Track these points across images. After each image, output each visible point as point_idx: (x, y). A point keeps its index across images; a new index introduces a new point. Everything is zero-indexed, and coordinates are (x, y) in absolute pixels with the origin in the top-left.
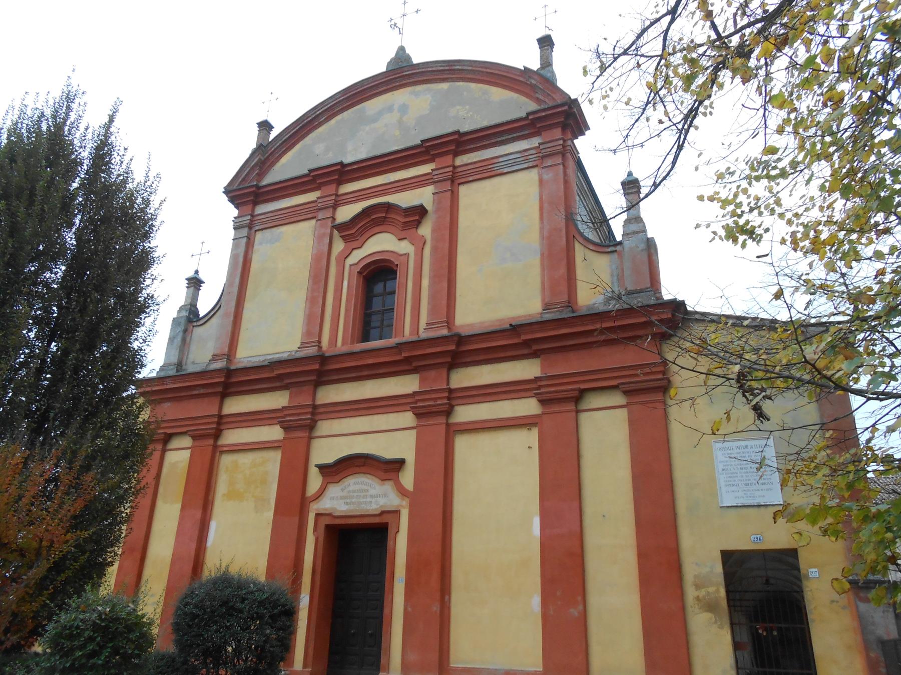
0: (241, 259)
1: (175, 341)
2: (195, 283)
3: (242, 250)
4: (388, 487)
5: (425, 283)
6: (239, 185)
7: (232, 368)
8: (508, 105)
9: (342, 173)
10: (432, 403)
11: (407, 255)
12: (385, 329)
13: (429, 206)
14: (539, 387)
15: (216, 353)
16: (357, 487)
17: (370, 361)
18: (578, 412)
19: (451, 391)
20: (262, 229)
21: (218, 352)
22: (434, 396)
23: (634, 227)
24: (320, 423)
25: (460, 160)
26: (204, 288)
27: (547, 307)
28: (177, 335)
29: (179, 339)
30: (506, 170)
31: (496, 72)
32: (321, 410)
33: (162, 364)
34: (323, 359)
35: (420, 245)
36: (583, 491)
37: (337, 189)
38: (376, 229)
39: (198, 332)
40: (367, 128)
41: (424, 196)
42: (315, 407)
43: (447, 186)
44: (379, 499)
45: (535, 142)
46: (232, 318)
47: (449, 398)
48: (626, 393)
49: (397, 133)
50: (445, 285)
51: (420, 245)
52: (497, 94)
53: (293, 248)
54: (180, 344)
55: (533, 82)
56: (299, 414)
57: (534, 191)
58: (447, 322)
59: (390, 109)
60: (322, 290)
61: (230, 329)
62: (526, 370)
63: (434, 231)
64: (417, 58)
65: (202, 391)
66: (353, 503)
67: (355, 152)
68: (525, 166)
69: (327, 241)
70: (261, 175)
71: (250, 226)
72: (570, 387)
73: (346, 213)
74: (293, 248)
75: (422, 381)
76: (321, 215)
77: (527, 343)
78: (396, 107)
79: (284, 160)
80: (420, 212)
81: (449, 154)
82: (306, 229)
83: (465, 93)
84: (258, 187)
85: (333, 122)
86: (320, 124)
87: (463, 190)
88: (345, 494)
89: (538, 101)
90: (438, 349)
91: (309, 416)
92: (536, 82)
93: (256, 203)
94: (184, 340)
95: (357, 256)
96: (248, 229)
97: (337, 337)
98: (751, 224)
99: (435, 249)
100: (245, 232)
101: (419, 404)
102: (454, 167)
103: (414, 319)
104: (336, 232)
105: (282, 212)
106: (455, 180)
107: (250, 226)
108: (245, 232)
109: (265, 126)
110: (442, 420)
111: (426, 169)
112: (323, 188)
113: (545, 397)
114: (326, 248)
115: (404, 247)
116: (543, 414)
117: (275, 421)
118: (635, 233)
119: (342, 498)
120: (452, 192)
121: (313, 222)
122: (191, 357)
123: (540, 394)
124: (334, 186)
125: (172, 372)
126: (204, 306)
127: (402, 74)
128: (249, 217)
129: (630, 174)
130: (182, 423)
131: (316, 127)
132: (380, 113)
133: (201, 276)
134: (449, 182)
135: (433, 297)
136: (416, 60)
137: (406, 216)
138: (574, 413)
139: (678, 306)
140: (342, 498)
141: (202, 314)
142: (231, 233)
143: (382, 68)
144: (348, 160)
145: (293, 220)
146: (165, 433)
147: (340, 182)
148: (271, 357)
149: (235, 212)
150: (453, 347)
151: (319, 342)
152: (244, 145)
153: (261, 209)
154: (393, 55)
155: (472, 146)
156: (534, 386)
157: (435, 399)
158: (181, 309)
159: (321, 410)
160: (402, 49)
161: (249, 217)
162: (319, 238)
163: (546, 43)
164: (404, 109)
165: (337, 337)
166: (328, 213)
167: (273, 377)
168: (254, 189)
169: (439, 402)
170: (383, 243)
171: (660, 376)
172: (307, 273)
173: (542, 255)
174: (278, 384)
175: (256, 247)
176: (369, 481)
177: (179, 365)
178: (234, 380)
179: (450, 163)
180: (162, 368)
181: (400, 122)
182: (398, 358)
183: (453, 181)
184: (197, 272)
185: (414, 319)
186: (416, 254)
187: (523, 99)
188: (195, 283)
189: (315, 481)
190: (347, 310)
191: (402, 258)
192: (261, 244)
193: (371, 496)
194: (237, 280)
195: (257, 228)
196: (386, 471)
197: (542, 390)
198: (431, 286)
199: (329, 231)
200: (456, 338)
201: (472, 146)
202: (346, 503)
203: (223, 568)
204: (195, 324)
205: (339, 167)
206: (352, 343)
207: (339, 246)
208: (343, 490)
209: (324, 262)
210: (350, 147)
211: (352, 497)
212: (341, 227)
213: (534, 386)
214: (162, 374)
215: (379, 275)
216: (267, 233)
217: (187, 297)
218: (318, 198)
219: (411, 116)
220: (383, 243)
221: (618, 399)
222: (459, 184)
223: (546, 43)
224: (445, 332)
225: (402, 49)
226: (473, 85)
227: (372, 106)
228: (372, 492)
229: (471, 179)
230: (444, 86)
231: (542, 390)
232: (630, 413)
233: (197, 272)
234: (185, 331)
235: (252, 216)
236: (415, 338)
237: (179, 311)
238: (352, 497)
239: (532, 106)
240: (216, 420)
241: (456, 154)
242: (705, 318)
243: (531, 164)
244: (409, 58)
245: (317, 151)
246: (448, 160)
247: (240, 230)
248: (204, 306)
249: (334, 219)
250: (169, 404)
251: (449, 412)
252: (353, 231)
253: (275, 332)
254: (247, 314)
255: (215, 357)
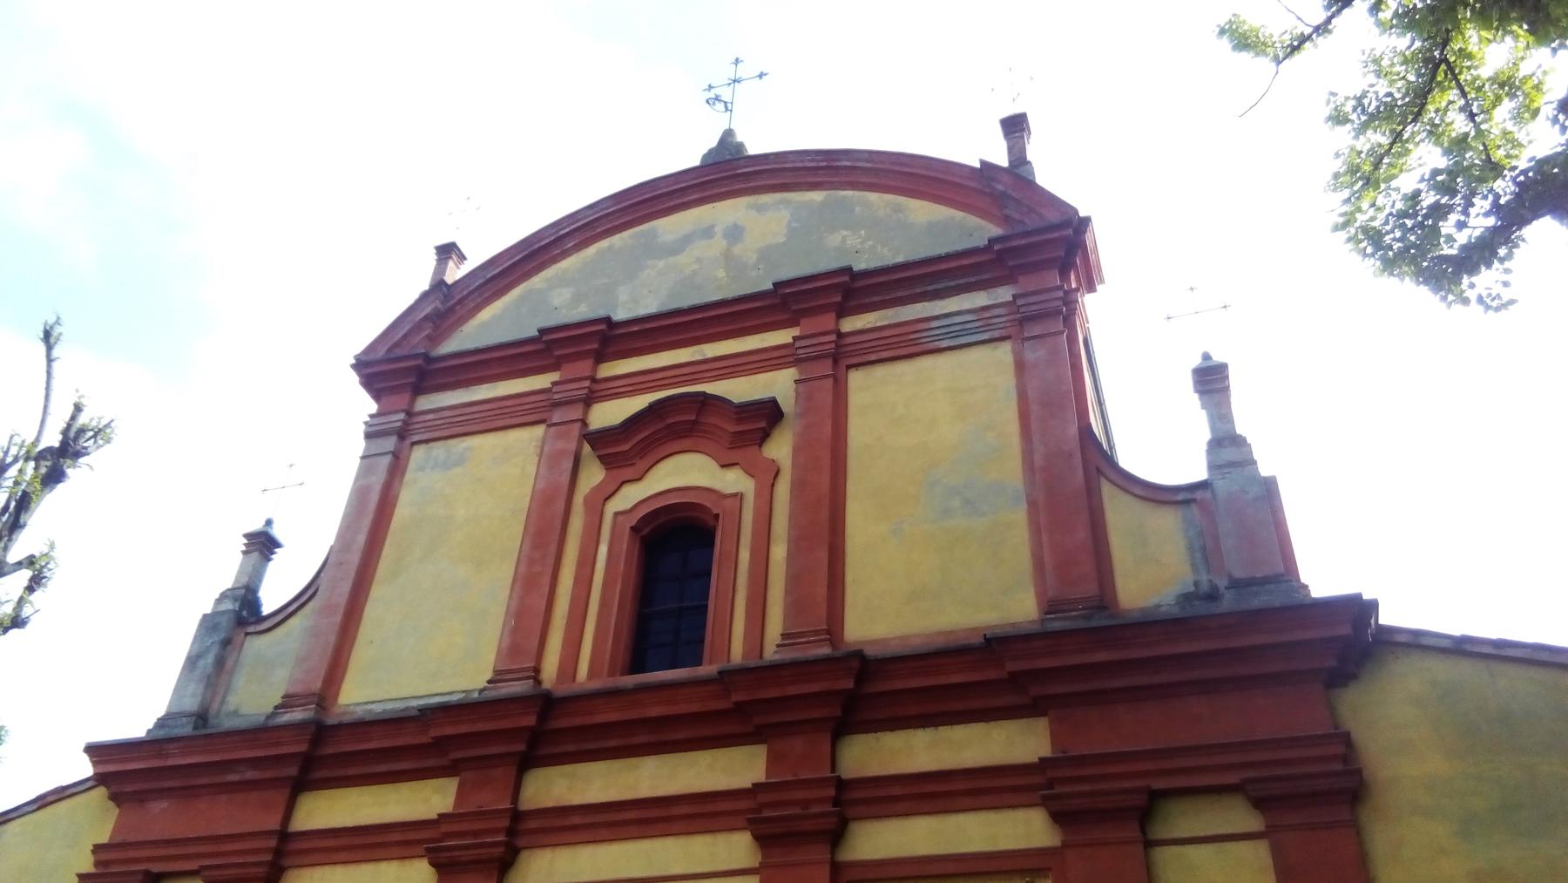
0: (374, 498)
1: (201, 663)
2: (263, 544)
3: (378, 480)
5: (779, 552)
6: (389, 350)
7: (331, 721)
8: (969, 230)
9: (609, 338)
10: (797, 811)
11: (739, 497)
12: (689, 647)
13: (787, 404)
14: (1050, 784)
15: (292, 690)
17: (655, 711)
18: (1149, 844)
19: (842, 784)
20: (427, 441)
21: (298, 689)
22: (800, 795)
23: (1229, 454)
24: (524, 855)
25: (851, 324)
26: (279, 556)
27: (1051, 607)
28: (208, 650)
29: (210, 659)
30: (945, 344)
31: (923, 172)
32: (533, 824)
33: (161, 712)
34: (546, 703)
35: (768, 476)
37: (595, 369)
38: (676, 446)
39: (256, 646)
40: (661, 264)
41: (779, 385)
42: (517, 816)
43: (826, 367)
45: (1004, 294)
46: (338, 618)
47: (836, 802)
48: (1260, 804)
49: (721, 273)
50: (823, 556)
51: (768, 476)
52: (922, 212)
53: (488, 480)
54: (210, 669)
55: (1000, 187)
56: (475, 834)
57: (1007, 382)
58: (828, 632)
59: (708, 232)
60: (550, 561)
61: (332, 639)
62: (1016, 742)
63: (797, 451)
64: (757, 143)
65: (250, 774)
67: (635, 300)
68: (986, 336)
69: (568, 464)
70: (435, 339)
71: (402, 434)
72: (1127, 784)
73: (609, 414)
74: (488, 480)
75: (773, 761)
76: (557, 416)
77: (1015, 681)
78: (718, 230)
79: (486, 314)
80: (767, 414)
81: (833, 315)
82: (525, 441)
83: (858, 209)
84: (428, 358)
85: (592, 250)
86: (565, 254)
87: (858, 381)
89: (1006, 220)
90: (815, 687)
91: (501, 838)
92: (1004, 190)
93: (419, 390)
94: (220, 663)
95: (631, 496)
96: (396, 440)
97: (576, 654)
99: (798, 486)
100: (390, 443)
101: (766, 813)
102: (840, 335)
103: (752, 621)
104: (587, 448)
105: (475, 409)
106: (843, 357)
107: (402, 434)
108: (390, 443)
109: (447, 252)
110: (820, 852)
111: (782, 337)
112: (564, 366)
114: (565, 479)
115: (733, 481)
116: (1065, 845)
117: (420, 850)
118: (1232, 464)
120: (836, 380)
121: (540, 430)
122: (233, 701)
123: (1058, 797)
124: (589, 363)
125: (186, 730)
126: (272, 597)
127: (728, 173)
128: (402, 416)
129: (1206, 357)
130: (191, 850)
131: (555, 260)
132: (687, 240)
133: (277, 532)
134: (829, 362)
135: (795, 580)
136: (752, 150)
137: (739, 421)
138: (1141, 847)
139: (1358, 610)
141: (267, 608)
142: (359, 445)
143: (694, 161)
144: (620, 315)
145: (493, 425)
146: (147, 873)
147: (601, 357)
148: (422, 702)
149: (373, 407)
150: (849, 684)
151: (537, 670)
152: (408, 282)
153: (426, 402)
154: (714, 143)
155: (875, 299)
156: (1038, 779)
157: (805, 803)
158: (224, 596)
159: (533, 824)
160: (729, 133)
161: (402, 416)
162: (548, 459)
163: (1015, 127)
164: (735, 233)
165: (576, 654)
166: (575, 413)
167: (429, 745)
168: (420, 362)
169: (815, 809)
170: (685, 472)
171: (1338, 767)
172: (518, 528)
173: (1032, 505)
174: (432, 762)
175: (409, 476)
177: (201, 717)
178: (329, 750)
179: (831, 326)
180: (161, 723)
181: (727, 256)
182: (721, 705)
183: (836, 362)
184: (269, 523)
185: (752, 621)
186: (758, 494)
187: (973, 221)
188: (263, 544)
190: (607, 584)
191: (729, 502)
192: (421, 469)
194: (361, 539)
195: (416, 438)
197: (1058, 790)
198: (791, 557)
199: (573, 446)
200: (855, 664)
201: (875, 299)
204: (251, 629)
205: (603, 327)
206: (612, 673)
207: (593, 475)
209: (560, 506)
210: (623, 294)
212: (601, 440)
213: (1038, 779)
214: (161, 734)
215: (676, 548)
216: (439, 450)
217: (240, 572)
218: (554, 384)
219: (750, 243)
220: (685, 472)
221: (1239, 816)
222: (849, 367)
223: (1015, 127)
224: (825, 651)
225: (729, 133)
226: (873, 197)
227: (670, 227)
229: (873, 357)
230: (817, 196)
231: (1058, 790)
232: (1277, 854)
233: (269, 523)
234: (226, 643)
235: (410, 413)
236: (752, 663)
237: (219, 601)
239: (995, 231)
240: (273, 843)
241: (842, 312)
242: (1417, 643)
243: (996, 334)
244: (740, 146)
245: (559, 297)
246: (826, 321)
247: (379, 441)
248: (272, 597)
249: (584, 423)
250: (165, 804)
251: (836, 836)
252: (625, 447)
253: (434, 646)
254: (374, 610)
255: (288, 702)
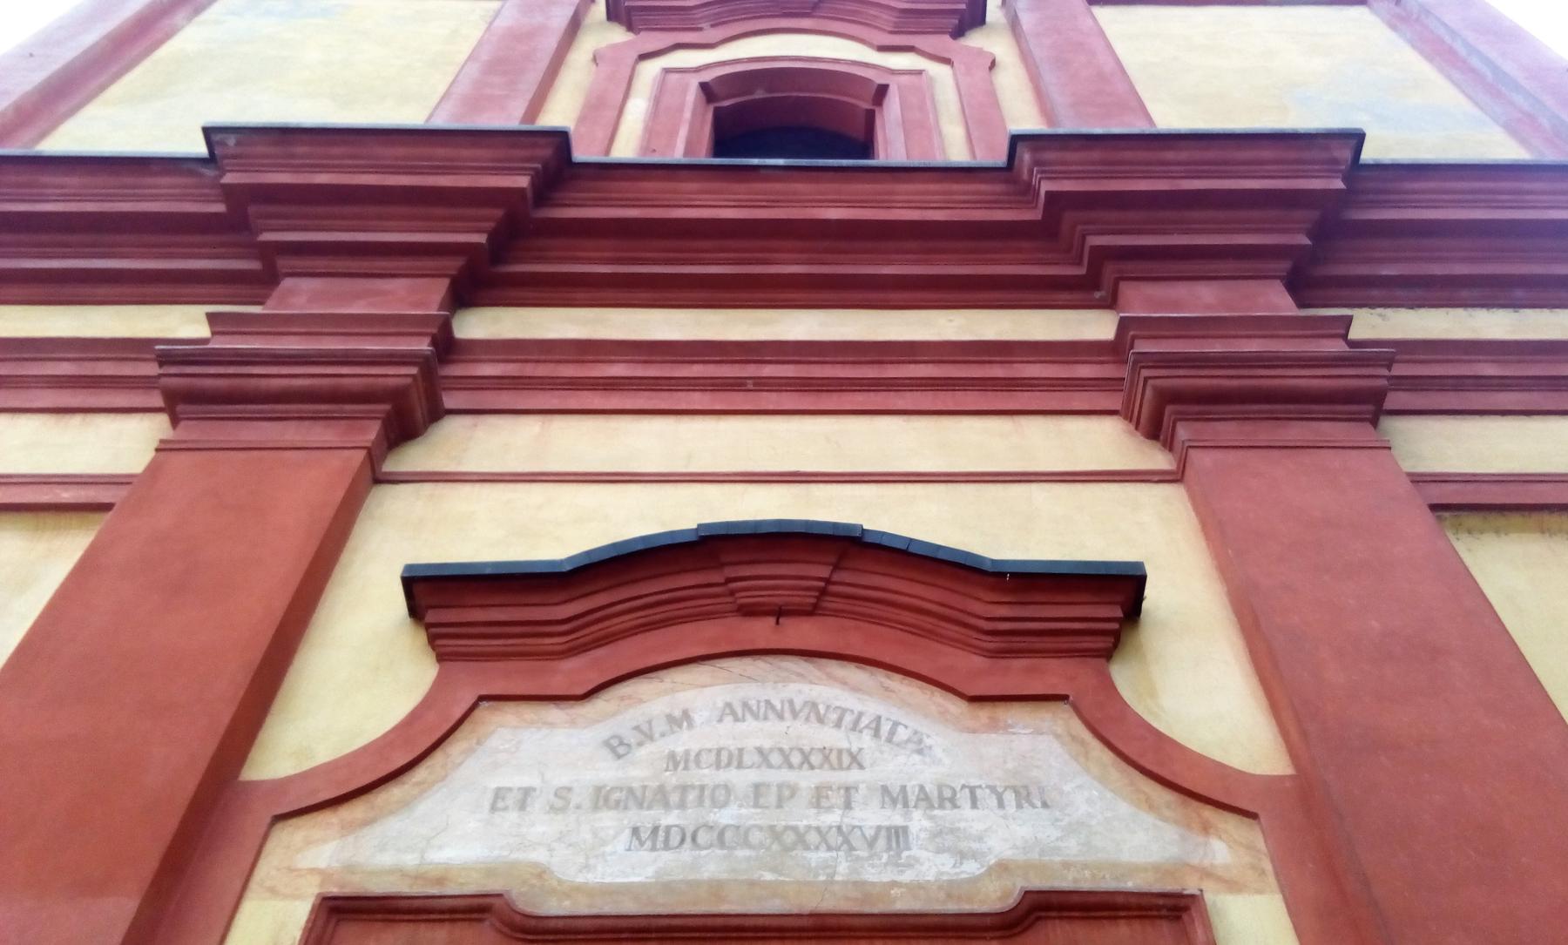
4: (1040, 743)
16: (756, 734)
36: (1498, 418)
44: (969, 819)
66: (742, 835)
88: (641, 769)
98: (909, 786)
113: (443, 650)
119: (602, 798)
140: (602, 798)
176: (872, 707)
189: (360, 671)
193: (894, 797)
196: (1010, 643)
202: (657, 838)
203: (334, 920)
208: (617, 748)
211: (721, 796)
228: (893, 767)
238: (721, 796)
251: (1123, 325)
